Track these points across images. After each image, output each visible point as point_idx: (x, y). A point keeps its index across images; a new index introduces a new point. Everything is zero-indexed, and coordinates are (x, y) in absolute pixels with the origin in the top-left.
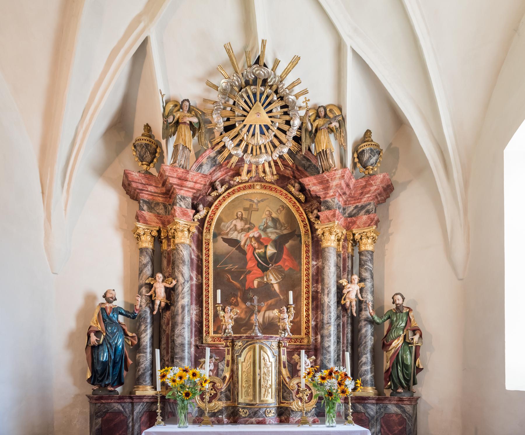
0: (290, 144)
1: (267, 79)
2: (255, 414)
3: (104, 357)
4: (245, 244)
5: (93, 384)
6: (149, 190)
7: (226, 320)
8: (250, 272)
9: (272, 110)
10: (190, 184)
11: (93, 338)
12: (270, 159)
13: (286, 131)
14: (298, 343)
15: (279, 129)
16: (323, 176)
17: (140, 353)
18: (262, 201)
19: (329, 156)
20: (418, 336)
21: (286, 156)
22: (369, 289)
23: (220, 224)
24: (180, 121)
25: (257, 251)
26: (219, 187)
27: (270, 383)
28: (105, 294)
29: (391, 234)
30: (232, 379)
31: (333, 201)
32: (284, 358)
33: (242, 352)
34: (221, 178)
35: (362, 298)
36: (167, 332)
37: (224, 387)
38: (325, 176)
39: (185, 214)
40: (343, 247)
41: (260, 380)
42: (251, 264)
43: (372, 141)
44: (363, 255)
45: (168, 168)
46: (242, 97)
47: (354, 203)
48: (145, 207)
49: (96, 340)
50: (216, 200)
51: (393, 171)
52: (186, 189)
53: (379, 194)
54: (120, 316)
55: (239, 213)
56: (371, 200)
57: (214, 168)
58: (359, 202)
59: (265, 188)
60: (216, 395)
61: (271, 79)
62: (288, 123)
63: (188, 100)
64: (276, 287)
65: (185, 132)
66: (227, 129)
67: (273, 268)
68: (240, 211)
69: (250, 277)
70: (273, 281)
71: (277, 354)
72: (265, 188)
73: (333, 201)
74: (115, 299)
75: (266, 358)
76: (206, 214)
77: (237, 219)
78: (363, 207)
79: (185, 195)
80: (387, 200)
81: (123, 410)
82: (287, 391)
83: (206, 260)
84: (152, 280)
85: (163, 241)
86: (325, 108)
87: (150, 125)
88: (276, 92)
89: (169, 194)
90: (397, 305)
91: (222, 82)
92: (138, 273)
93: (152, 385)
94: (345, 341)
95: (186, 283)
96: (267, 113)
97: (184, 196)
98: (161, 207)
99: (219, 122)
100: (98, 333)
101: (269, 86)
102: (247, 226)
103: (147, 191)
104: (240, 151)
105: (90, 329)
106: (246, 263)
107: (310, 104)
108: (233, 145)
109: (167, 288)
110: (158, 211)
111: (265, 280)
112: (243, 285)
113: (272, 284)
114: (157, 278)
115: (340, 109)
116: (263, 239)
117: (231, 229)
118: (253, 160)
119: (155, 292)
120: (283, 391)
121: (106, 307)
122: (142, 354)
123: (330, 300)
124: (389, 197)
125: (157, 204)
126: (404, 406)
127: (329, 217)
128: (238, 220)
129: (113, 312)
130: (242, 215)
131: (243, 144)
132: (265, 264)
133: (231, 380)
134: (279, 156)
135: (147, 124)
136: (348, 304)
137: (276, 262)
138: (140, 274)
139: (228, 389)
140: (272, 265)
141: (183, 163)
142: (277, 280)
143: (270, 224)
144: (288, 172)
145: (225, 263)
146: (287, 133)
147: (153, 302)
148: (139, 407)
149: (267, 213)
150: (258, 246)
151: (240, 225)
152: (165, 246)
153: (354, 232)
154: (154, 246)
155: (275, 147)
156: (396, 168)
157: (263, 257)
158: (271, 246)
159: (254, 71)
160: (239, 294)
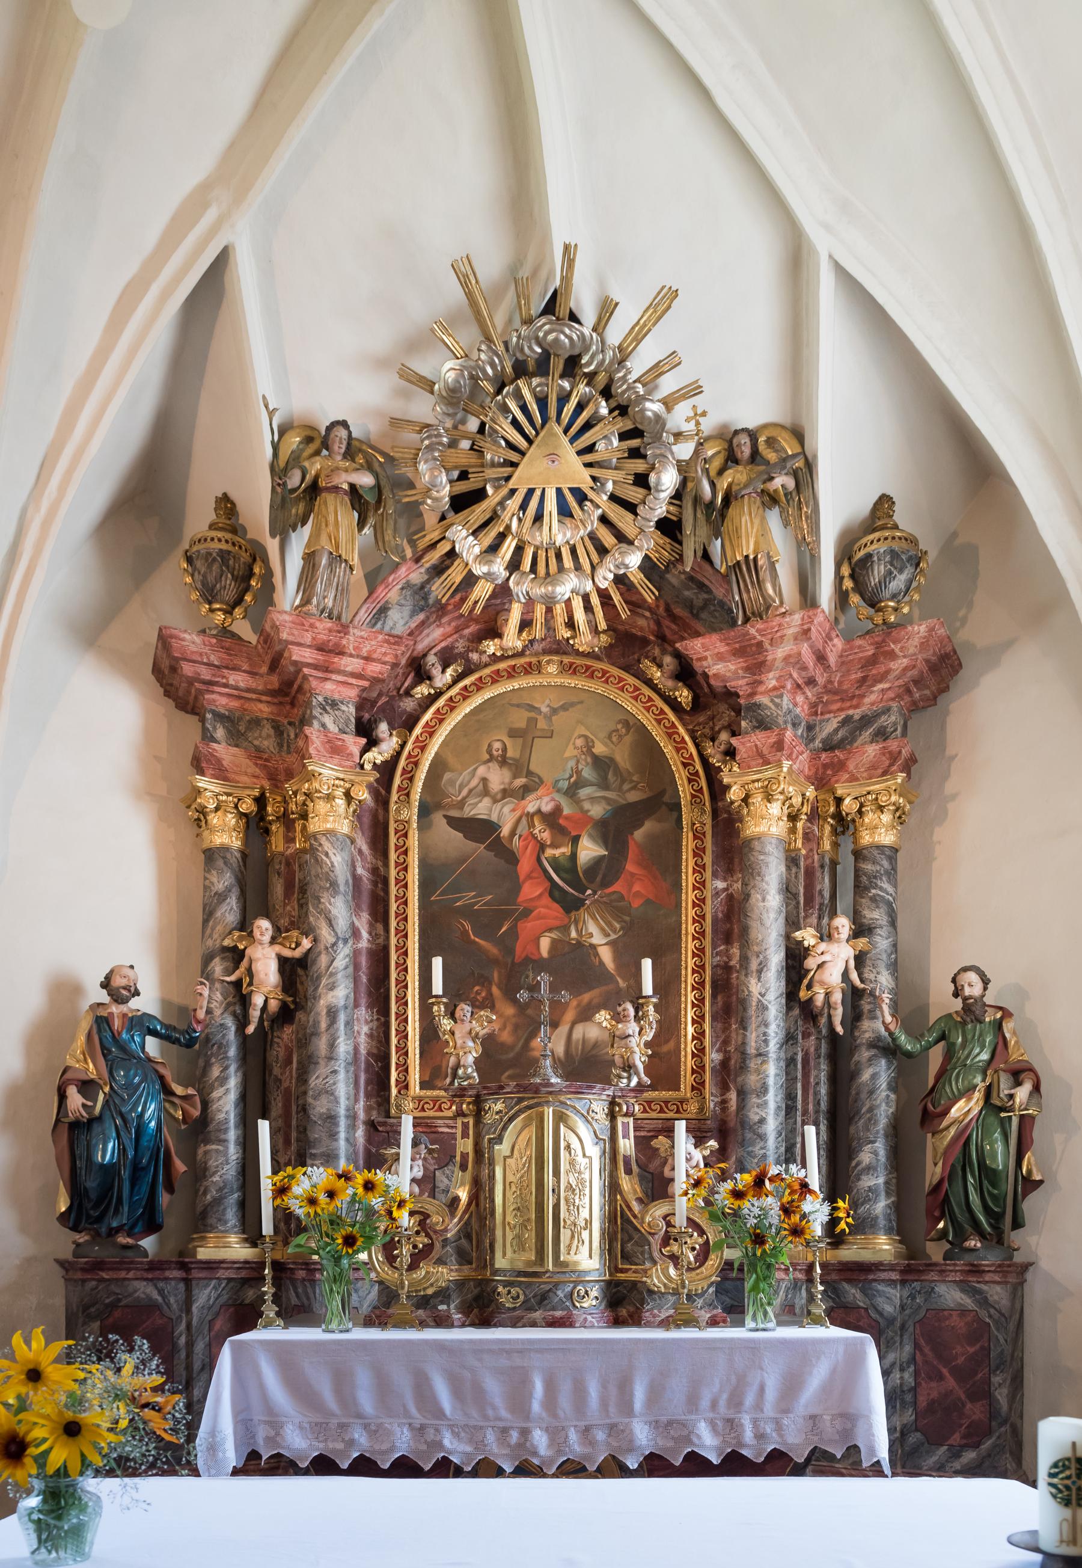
2: (543, 1299)
3: (107, 1152)
4: (513, 833)
5: (75, 1228)
6: (231, 682)
7: (459, 1042)
8: (527, 913)
9: (594, 444)
10: (351, 664)
11: (75, 1100)
12: (589, 586)
16: (747, 633)
17: (207, 1142)
18: (564, 708)
19: (764, 574)
22: (884, 957)
23: (440, 777)
24: (322, 483)
25: (549, 852)
26: (436, 671)
27: (585, 1214)
28: (108, 978)
30: (477, 1205)
31: (777, 705)
32: (627, 1145)
33: (505, 1128)
34: (443, 644)
35: (862, 981)
36: (286, 1084)
37: (453, 1227)
38: (753, 631)
39: (335, 749)
40: (807, 837)
42: (531, 891)
43: (896, 527)
44: (865, 859)
45: (287, 618)
47: (841, 710)
48: (220, 733)
50: (428, 707)
52: (340, 678)
55: (497, 745)
56: (893, 699)
58: (856, 707)
60: (429, 1248)
62: (641, 480)
63: (344, 424)
64: (606, 955)
66: (461, 502)
67: (596, 901)
69: (527, 927)
70: (598, 939)
73: (777, 705)
74: (137, 993)
75: (575, 1144)
77: (489, 761)
78: (866, 721)
79: (336, 697)
81: (160, 1299)
82: (636, 1237)
83: (397, 881)
85: (274, 828)
87: (234, 495)
90: (965, 999)
93: (244, 1232)
94: (811, 1107)
95: (340, 944)
97: (336, 695)
98: (268, 730)
100: (87, 1087)
102: (520, 781)
103: (226, 686)
104: (499, 567)
106: (517, 888)
107: (708, 425)
108: (477, 550)
110: (256, 743)
111: (574, 934)
112: (510, 951)
113: (593, 947)
115: (798, 435)
116: (567, 818)
117: (470, 791)
118: (539, 591)
120: (622, 1236)
121: (111, 1014)
122: (214, 1147)
123: (767, 988)
124: (946, 689)
125: (256, 722)
126: (984, 1287)
127: (765, 751)
128: (494, 766)
130: (505, 749)
132: (572, 889)
135: (225, 495)
136: (819, 1000)
137: (605, 884)
138: (205, 922)
139: (466, 1232)
140: (595, 893)
141: (330, 604)
142: (607, 935)
143: (587, 773)
144: (643, 624)
145: (455, 888)
146: (640, 510)
149: (580, 742)
151: (497, 778)
152: (277, 843)
153: (840, 792)
154: (246, 841)
155: (603, 551)
157: (566, 871)
158: (591, 836)
159: (541, 334)
160: (496, 975)
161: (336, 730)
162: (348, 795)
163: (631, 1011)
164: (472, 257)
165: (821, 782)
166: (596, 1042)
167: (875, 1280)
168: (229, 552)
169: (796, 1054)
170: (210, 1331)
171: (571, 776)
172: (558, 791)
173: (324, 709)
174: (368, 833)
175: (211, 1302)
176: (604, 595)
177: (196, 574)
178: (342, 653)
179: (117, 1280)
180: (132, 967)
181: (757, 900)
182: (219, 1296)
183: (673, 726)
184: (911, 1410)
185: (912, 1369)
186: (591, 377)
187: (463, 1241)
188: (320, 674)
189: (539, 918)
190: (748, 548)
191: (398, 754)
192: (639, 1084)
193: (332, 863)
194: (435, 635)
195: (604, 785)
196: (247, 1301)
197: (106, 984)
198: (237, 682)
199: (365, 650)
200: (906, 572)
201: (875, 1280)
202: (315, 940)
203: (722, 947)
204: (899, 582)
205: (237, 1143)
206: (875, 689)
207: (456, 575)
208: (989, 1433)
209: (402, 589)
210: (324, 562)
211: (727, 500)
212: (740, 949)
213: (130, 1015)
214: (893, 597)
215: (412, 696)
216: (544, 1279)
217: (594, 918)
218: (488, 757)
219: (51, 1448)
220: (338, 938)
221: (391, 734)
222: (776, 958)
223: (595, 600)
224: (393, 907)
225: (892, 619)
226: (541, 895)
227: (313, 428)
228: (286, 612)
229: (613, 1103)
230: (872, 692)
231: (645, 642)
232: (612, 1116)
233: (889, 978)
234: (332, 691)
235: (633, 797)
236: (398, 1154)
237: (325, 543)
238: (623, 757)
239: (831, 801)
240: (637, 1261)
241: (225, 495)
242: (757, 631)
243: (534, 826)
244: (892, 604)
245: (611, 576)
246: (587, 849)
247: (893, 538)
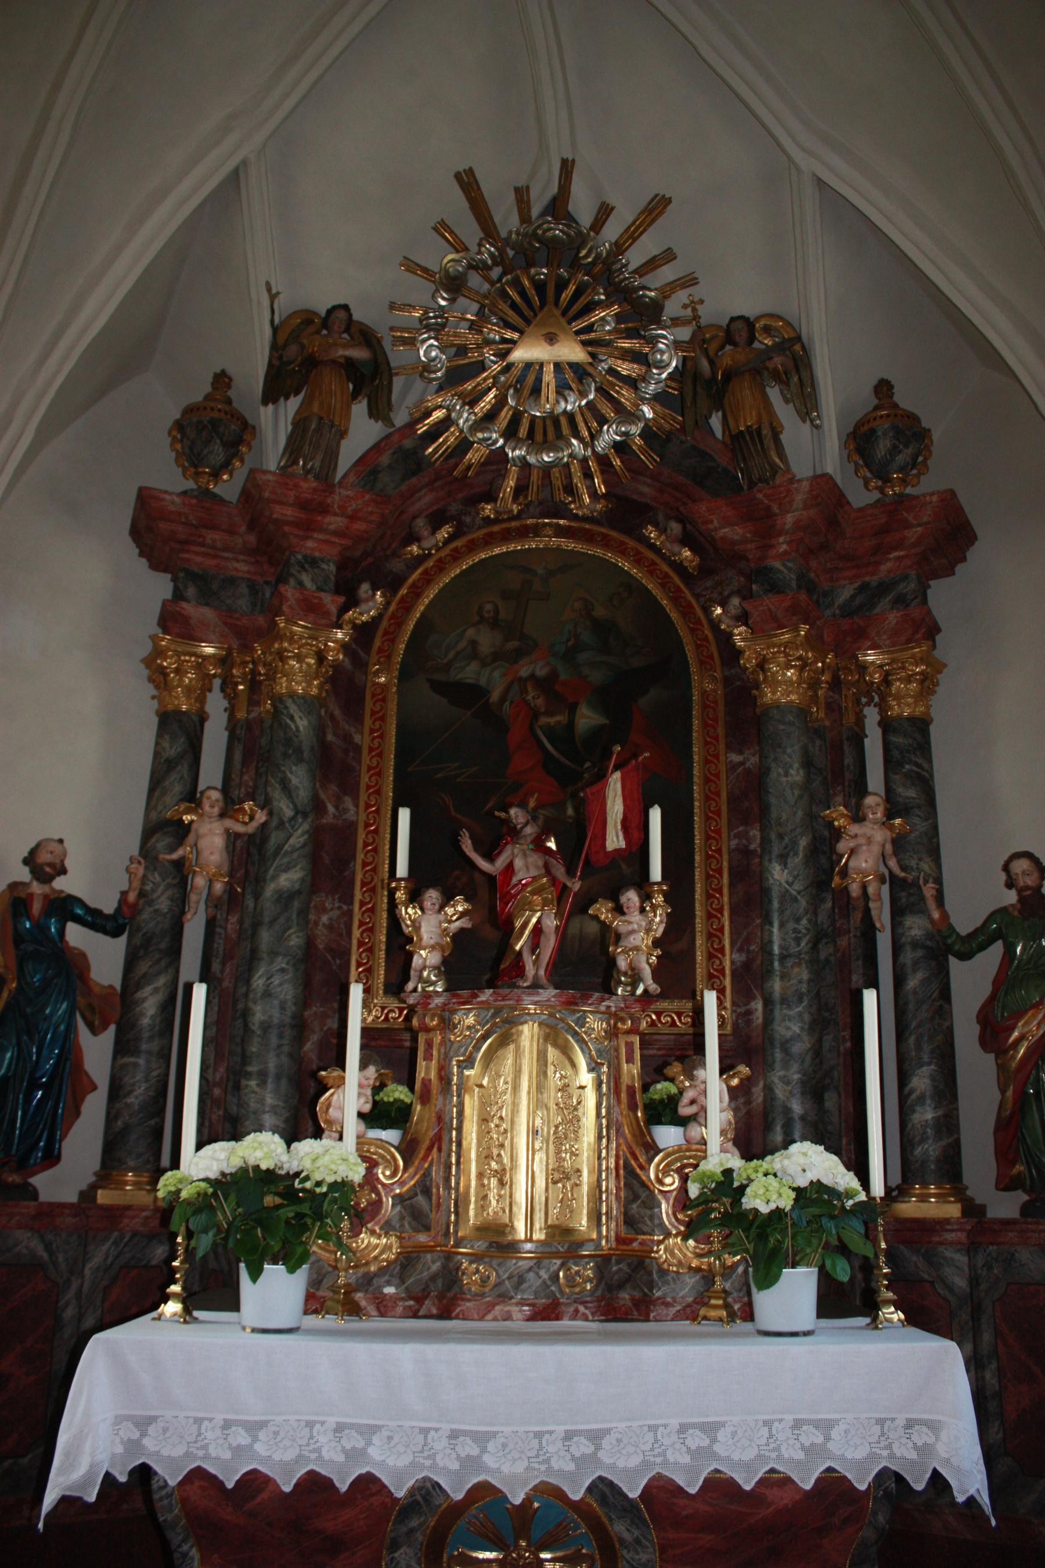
4: (503, 699)
10: (335, 522)
19: (769, 443)
25: (544, 720)
28: (33, 852)
33: (477, 1048)
35: (903, 868)
38: (760, 496)
39: (310, 608)
45: (270, 477)
48: (191, 591)
50: (416, 568)
52: (321, 537)
55: (488, 607)
63: (346, 307)
74: (63, 871)
78: (883, 588)
81: (45, 1256)
82: (643, 1196)
90: (1020, 892)
91: (445, 261)
98: (244, 589)
103: (203, 545)
109: (238, 835)
110: (229, 602)
117: (458, 654)
125: (231, 581)
130: (497, 611)
136: (855, 889)
144: (645, 490)
148: (105, 1248)
151: (487, 640)
159: (540, 232)
161: (314, 588)
167: (941, 1243)
170: (103, 1301)
171: (568, 640)
173: (303, 567)
175: (109, 1262)
177: (185, 441)
180: (61, 841)
181: (779, 775)
182: (120, 1253)
184: (997, 1424)
185: (994, 1365)
186: (589, 269)
188: (301, 533)
190: (748, 420)
192: (646, 991)
193: (297, 727)
196: (154, 1263)
198: (214, 541)
199: (350, 509)
201: (941, 1243)
203: (741, 829)
206: (892, 556)
209: (394, 453)
210: (313, 426)
211: (728, 376)
212: (761, 830)
213: (52, 897)
214: (900, 470)
215: (399, 557)
218: (477, 618)
219: (199, 1180)
220: (297, 812)
228: (270, 472)
230: (888, 560)
234: (313, 549)
236: (344, 1078)
240: (645, 1229)
242: (765, 495)
243: (527, 692)
247: (896, 415)
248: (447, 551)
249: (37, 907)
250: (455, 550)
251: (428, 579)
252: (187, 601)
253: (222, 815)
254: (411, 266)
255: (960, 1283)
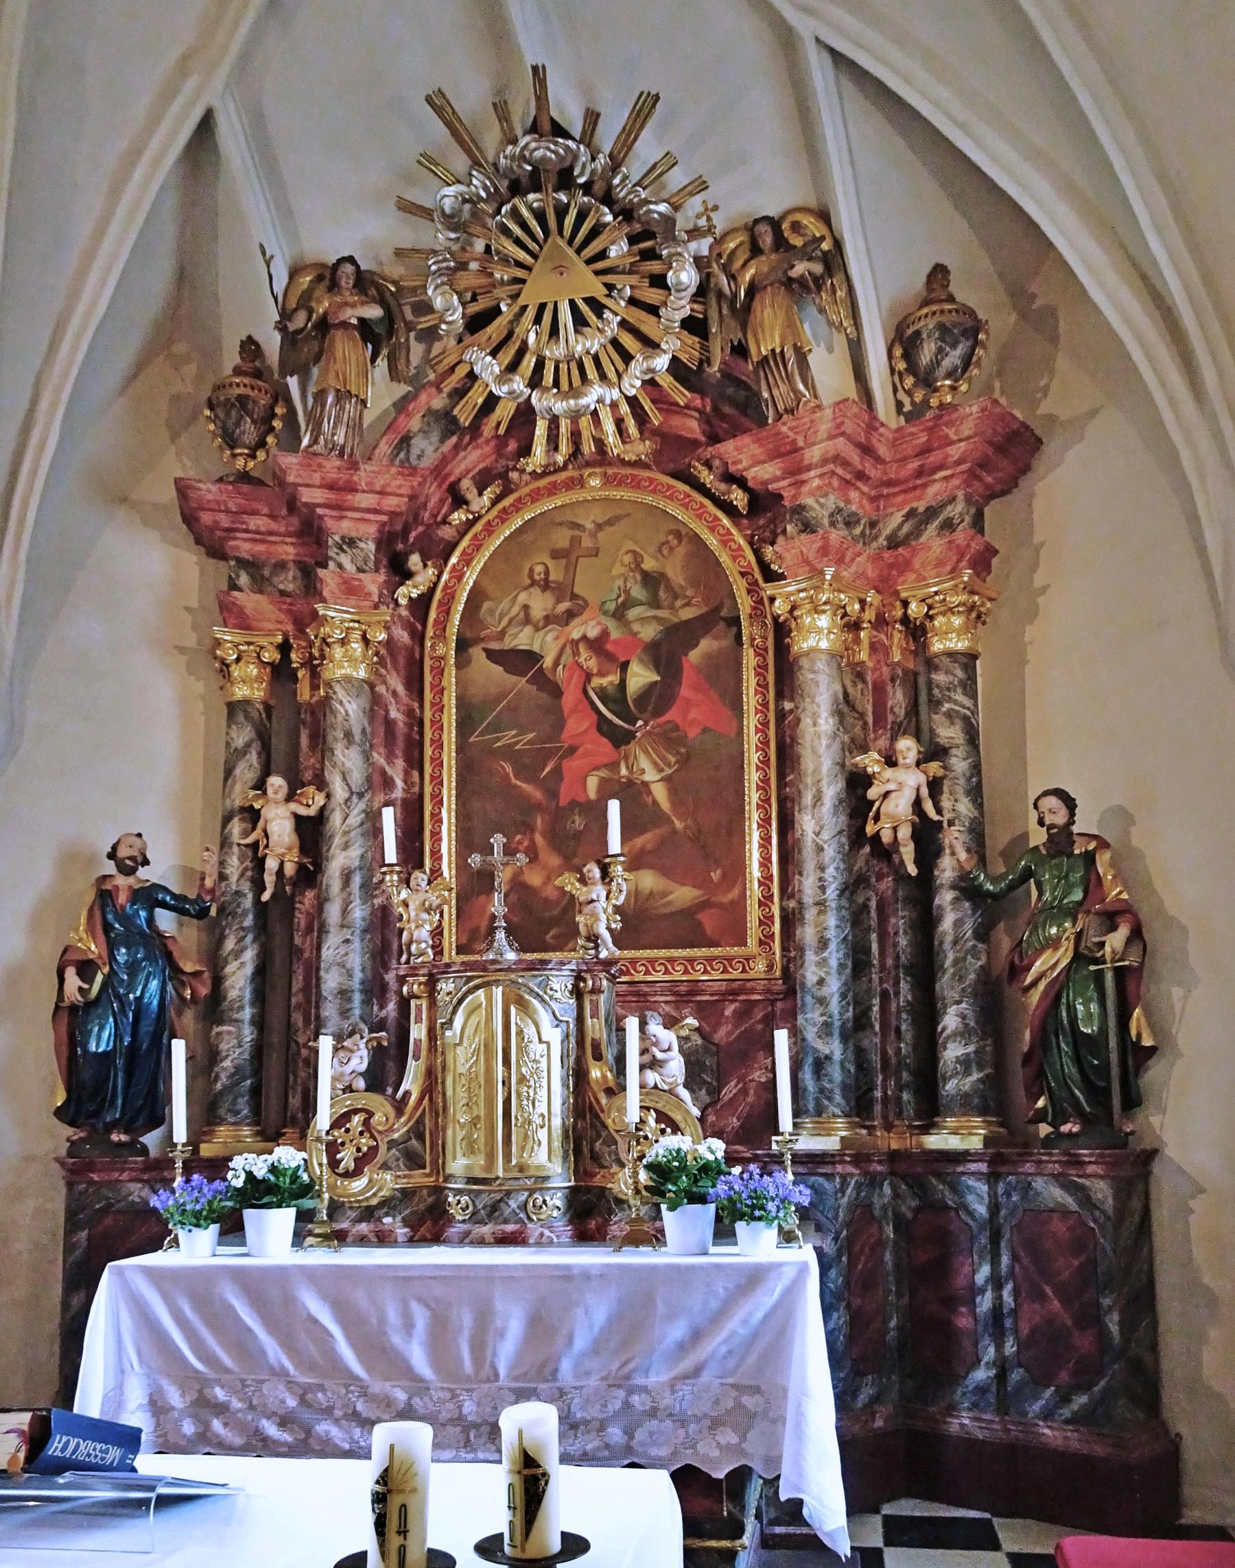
0: (673, 344)
1: (571, 168)
3: (101, 1040)
4: (556, 663)
5: (72, 1123)
6: (252, 527)
7: (413, 914)
8: (572, 750)
9: (605, 251)
10: (365, 500)
11: (73, 980)
12: (615, 394)
13: (657, 308)
14: (735, 974)
15: (632, 301)
16: (779, 433)
17: (220, 1022)
18: (610, 522)
20: (1123, 932)
21: (666, 381)
22: (962, 781)
23: (479, 607)
24: (333, 320)
25: (596, 682)
26: (471, 494)
27: (542, 1108)
28: (114, 848)
29: (1043, 590)
30: (431, 1099)
31: (822, 506)
33: (454, 1012)
34: (481, 466)
36: (306, 955)
37: (401, 1129)
38: (784, 429)
39: (351, 590)
40: (873, 647)
41: (507, 1102)
42: (578, 725)
43: (951, 299)
44: (936, 668)
46: (505, 231)
47: (904, 503)
48: (244, 579)
49: (80, 989)
51: (1042, 383)
53: (982, 465)
54: (158, 910)
55: (539, 569)
56: (958, 487)
57: (454, 439)
58: (920, 498)
59: (619, 485)
60: (374, 1150)
61: (584, 166)
62: (659, 281)
63: (351, 260)
64: (660, 793)
65: (347, 351)
66: (476, 323)
67: (649, 733)
68: (539, 562)
69: (572, 765)
70: (650, 775)
71: (570, 1017)
72: (618, 482)
73: (822, 506)
74: (146, 862)
75: (530, 1031)
76: (434, 579)
77: (531, 585)
78: (931, 513)
79: (354, 534)
80: (1024, 482)
82: (604, 1134)
83: (433, 723)
84: (257, 797)
85: (300, 674)
86: (774, 224)
87: (256, 337)
88: (608, 199)
89: (311, 532)
92: (221, 775)
93: (257, 1123)
94: (890, 962)
95: (355, 799)
96: (589, 262)
97: (356, 532)
99: (450, 309)
100: (86, 969)
101: (581, 186)
102: (564, 606)
103: (247, 531)
104: (519, 384)
105: (66, 957)
106: (560, 724)
107: (720, 222)
108: (497, 370)
110: (281, 587)
111: (624, 771)
112: (553, 794)
113: (646, 784)
114: (270, 791)
115: (824, 216)
116: (616, 642)
117: (511, 620)
118: (560, 407)
119: (265, 831)
120: (587, 1134)
121: (117, 887)
122: (225, 1028)
123: (820, 824)
124: (1026, 469)
125: (281, 566)
126: (1087, 1182)
127: (811, 556)
128: (535, 591)
129: (133, 903)
130: (547, 572)
131: (529, 362)
132: (620, 721)
133: (426, 1102)
134: (644, 382)
135: (250, 338)
136: (886, 837)
137: (657, 714)
138: (226, 780)
139: (417, 1132)
140: (646, 724)
141: (342, 441)
142: (661, 770)
143: (638, 592)
145: (495, 727)
146: (662, 311)
147: (259, 864)
149: (628, 559)
150: (600, 664)
151: (540, 604)
152: (304, 692)
153: (903, 595)
154: (272, 690)
156: (1051, 372)
157: (615, 701)
158: (641, 661)
160: (539, 821)
162: (365, 640)
163: (597, 873)
164: (444, 90)
165: (885, 585)
166: (651, 893)
167: (964, 1173)
168: (247, 397)
169: (868, 899)
172: (605, 613)
174: (403, 672)
176: (633, 402)
178: (354, 490)
179: (109, 1182)
180: (139, 835)
183: (729, 533)
186: (587, 188)
187: (414, 1142)
188: (334, 513)
189: (584, 756)
191: (432, 591)
194: (473, 458)
195: (655, 603)
197: (112, 855)
200: (960, 346)
202: (328, 796)
204: (953, 358)
205: (253, 1022)
207: (477, 397)
208: (1100, 1372)
211: (752, 290)
214: (949, 375)
216: (494, 1187)
217: (646, 752)
221: (425, 566)
222: (832, 790)
223: (625, 409)
224: (428, 751)
225: (949, 399)
226: (586, 731)
227: (323, 266)
229: (579, 977)
231: (695, 444)
232: (577, 993)
233: (970, 805)
235: (687, 614)
237: (332, 382)
238: (675, 571)
239: (898, 604)
241: (250, 338)
243: (579, 654)
244: (948, 382)
245: (638, 383)
246: (638, 675)
248: (494, 512)
249: (122, 898)
250: (504, 510)
251: (477, 546)
252: (240, 590)
253: (290, 798)
254: (409, 208)
255: (981, 1210)
